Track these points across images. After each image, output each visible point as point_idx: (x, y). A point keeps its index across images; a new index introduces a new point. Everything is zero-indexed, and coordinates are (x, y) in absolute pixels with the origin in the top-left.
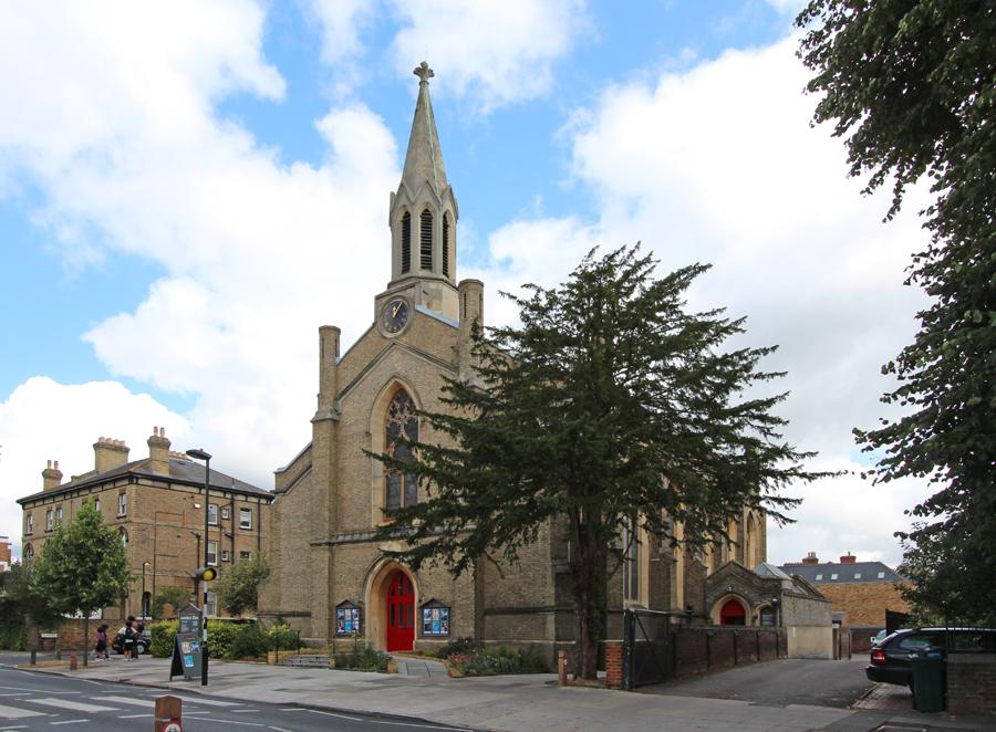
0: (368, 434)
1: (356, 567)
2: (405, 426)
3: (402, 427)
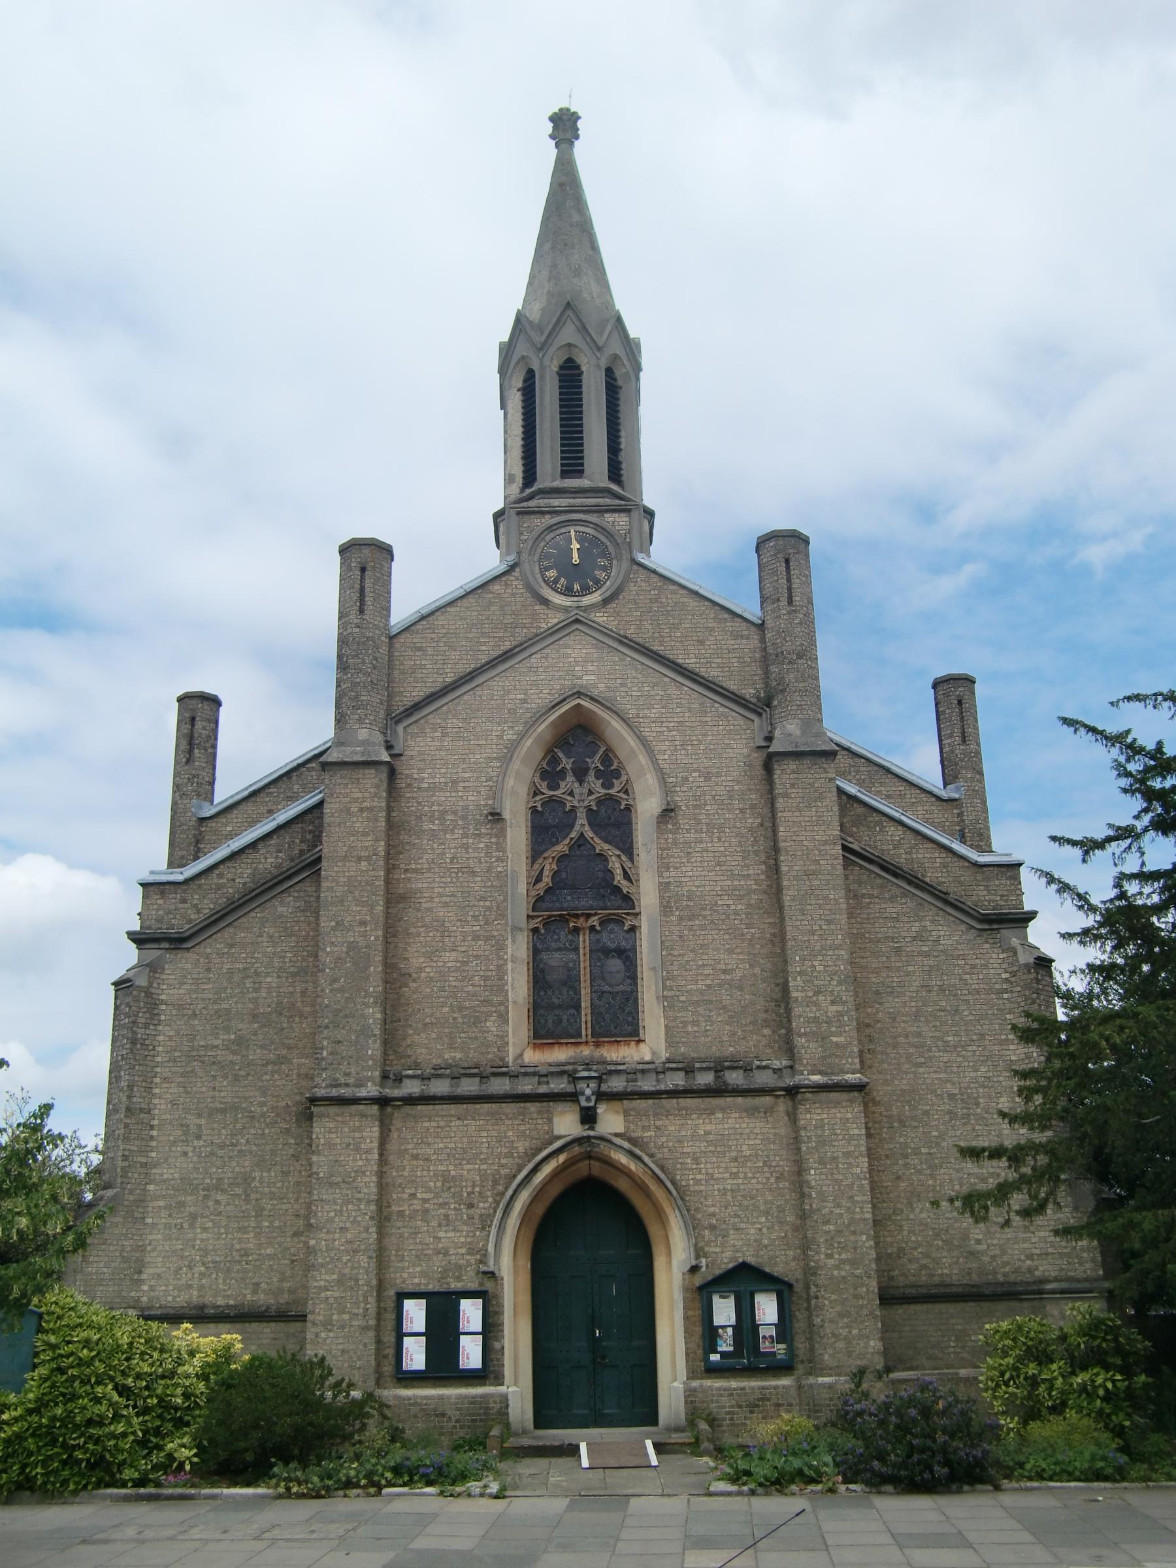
0: (496, 817)
1: (470, 1172)
2: (589, 810)
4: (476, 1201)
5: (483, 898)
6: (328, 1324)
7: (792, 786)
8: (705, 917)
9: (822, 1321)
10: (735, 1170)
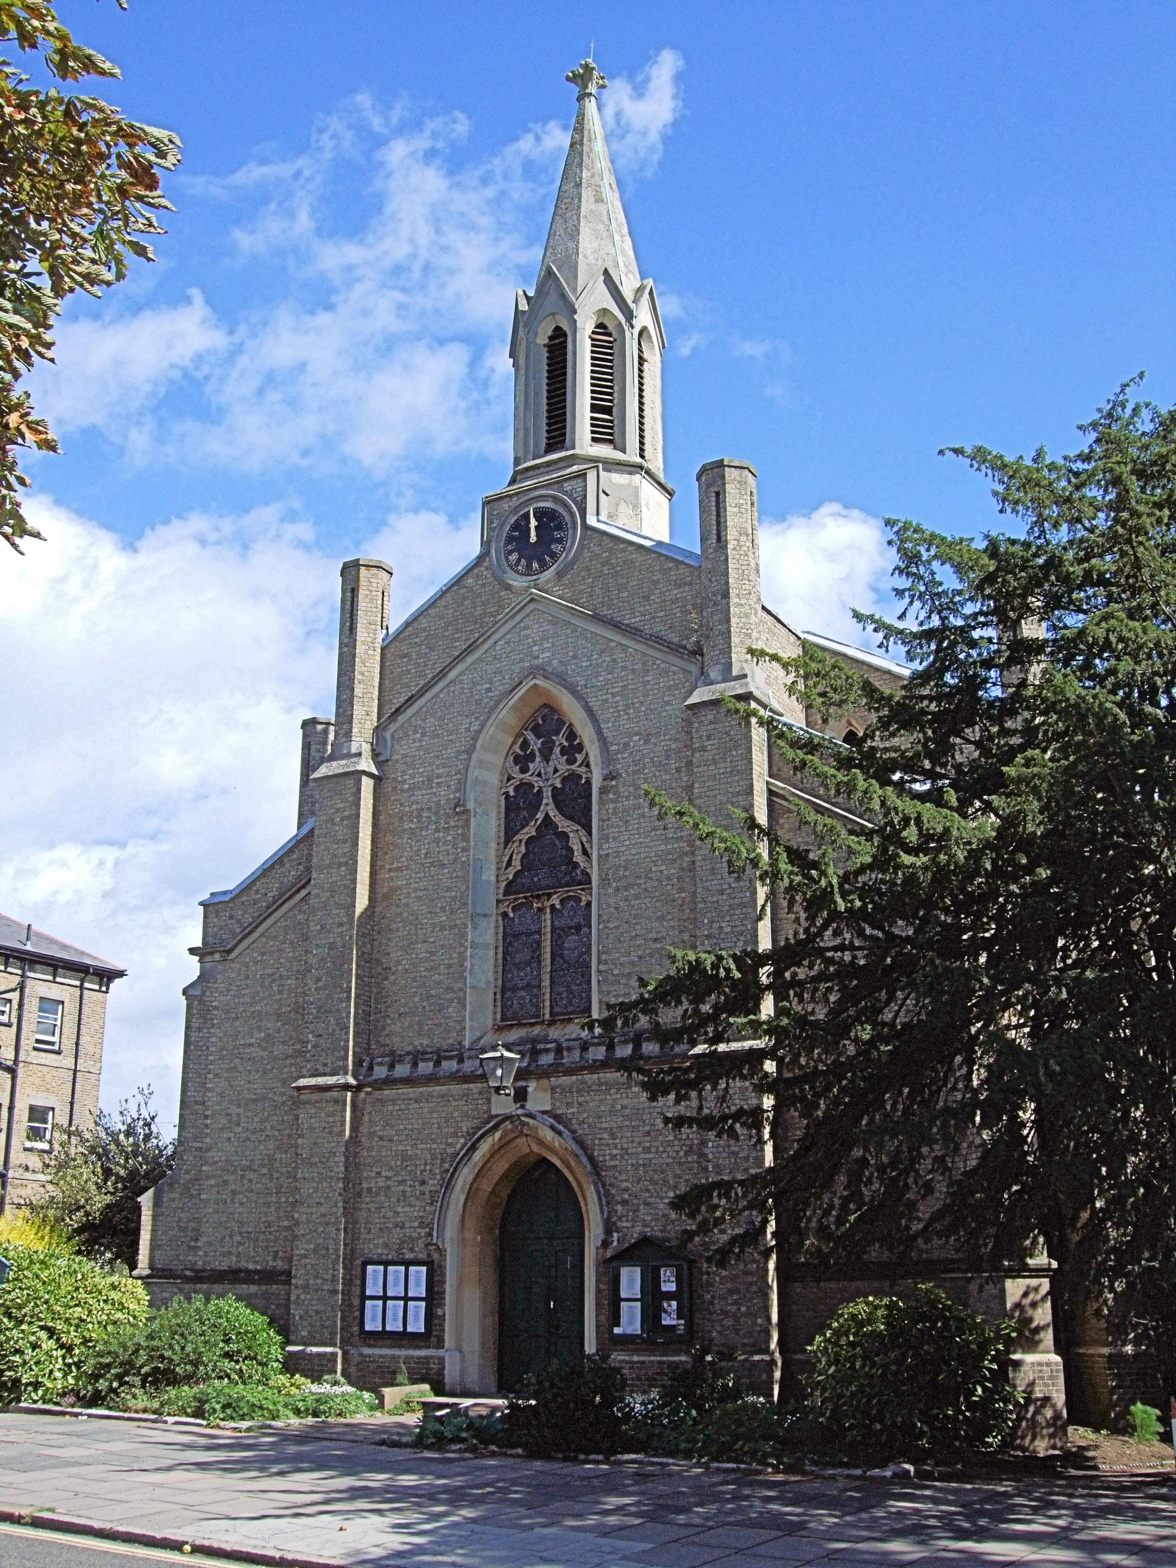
0: (459, 809)
3: (547, 793)
4: (426, 1178)
5: (449, 889)
6: (306, 1287)
7: (709, 738)
8: (639, 885)
9: (713, 1297)
10: (648, 1144)
